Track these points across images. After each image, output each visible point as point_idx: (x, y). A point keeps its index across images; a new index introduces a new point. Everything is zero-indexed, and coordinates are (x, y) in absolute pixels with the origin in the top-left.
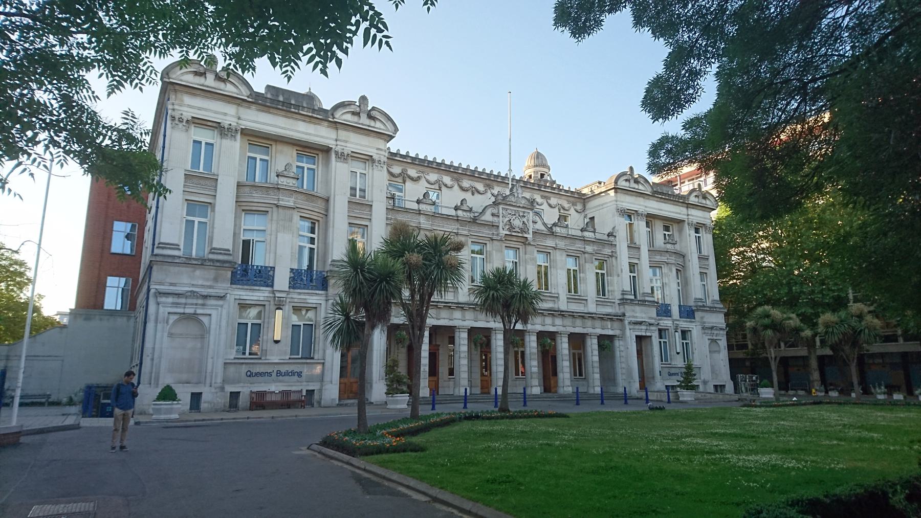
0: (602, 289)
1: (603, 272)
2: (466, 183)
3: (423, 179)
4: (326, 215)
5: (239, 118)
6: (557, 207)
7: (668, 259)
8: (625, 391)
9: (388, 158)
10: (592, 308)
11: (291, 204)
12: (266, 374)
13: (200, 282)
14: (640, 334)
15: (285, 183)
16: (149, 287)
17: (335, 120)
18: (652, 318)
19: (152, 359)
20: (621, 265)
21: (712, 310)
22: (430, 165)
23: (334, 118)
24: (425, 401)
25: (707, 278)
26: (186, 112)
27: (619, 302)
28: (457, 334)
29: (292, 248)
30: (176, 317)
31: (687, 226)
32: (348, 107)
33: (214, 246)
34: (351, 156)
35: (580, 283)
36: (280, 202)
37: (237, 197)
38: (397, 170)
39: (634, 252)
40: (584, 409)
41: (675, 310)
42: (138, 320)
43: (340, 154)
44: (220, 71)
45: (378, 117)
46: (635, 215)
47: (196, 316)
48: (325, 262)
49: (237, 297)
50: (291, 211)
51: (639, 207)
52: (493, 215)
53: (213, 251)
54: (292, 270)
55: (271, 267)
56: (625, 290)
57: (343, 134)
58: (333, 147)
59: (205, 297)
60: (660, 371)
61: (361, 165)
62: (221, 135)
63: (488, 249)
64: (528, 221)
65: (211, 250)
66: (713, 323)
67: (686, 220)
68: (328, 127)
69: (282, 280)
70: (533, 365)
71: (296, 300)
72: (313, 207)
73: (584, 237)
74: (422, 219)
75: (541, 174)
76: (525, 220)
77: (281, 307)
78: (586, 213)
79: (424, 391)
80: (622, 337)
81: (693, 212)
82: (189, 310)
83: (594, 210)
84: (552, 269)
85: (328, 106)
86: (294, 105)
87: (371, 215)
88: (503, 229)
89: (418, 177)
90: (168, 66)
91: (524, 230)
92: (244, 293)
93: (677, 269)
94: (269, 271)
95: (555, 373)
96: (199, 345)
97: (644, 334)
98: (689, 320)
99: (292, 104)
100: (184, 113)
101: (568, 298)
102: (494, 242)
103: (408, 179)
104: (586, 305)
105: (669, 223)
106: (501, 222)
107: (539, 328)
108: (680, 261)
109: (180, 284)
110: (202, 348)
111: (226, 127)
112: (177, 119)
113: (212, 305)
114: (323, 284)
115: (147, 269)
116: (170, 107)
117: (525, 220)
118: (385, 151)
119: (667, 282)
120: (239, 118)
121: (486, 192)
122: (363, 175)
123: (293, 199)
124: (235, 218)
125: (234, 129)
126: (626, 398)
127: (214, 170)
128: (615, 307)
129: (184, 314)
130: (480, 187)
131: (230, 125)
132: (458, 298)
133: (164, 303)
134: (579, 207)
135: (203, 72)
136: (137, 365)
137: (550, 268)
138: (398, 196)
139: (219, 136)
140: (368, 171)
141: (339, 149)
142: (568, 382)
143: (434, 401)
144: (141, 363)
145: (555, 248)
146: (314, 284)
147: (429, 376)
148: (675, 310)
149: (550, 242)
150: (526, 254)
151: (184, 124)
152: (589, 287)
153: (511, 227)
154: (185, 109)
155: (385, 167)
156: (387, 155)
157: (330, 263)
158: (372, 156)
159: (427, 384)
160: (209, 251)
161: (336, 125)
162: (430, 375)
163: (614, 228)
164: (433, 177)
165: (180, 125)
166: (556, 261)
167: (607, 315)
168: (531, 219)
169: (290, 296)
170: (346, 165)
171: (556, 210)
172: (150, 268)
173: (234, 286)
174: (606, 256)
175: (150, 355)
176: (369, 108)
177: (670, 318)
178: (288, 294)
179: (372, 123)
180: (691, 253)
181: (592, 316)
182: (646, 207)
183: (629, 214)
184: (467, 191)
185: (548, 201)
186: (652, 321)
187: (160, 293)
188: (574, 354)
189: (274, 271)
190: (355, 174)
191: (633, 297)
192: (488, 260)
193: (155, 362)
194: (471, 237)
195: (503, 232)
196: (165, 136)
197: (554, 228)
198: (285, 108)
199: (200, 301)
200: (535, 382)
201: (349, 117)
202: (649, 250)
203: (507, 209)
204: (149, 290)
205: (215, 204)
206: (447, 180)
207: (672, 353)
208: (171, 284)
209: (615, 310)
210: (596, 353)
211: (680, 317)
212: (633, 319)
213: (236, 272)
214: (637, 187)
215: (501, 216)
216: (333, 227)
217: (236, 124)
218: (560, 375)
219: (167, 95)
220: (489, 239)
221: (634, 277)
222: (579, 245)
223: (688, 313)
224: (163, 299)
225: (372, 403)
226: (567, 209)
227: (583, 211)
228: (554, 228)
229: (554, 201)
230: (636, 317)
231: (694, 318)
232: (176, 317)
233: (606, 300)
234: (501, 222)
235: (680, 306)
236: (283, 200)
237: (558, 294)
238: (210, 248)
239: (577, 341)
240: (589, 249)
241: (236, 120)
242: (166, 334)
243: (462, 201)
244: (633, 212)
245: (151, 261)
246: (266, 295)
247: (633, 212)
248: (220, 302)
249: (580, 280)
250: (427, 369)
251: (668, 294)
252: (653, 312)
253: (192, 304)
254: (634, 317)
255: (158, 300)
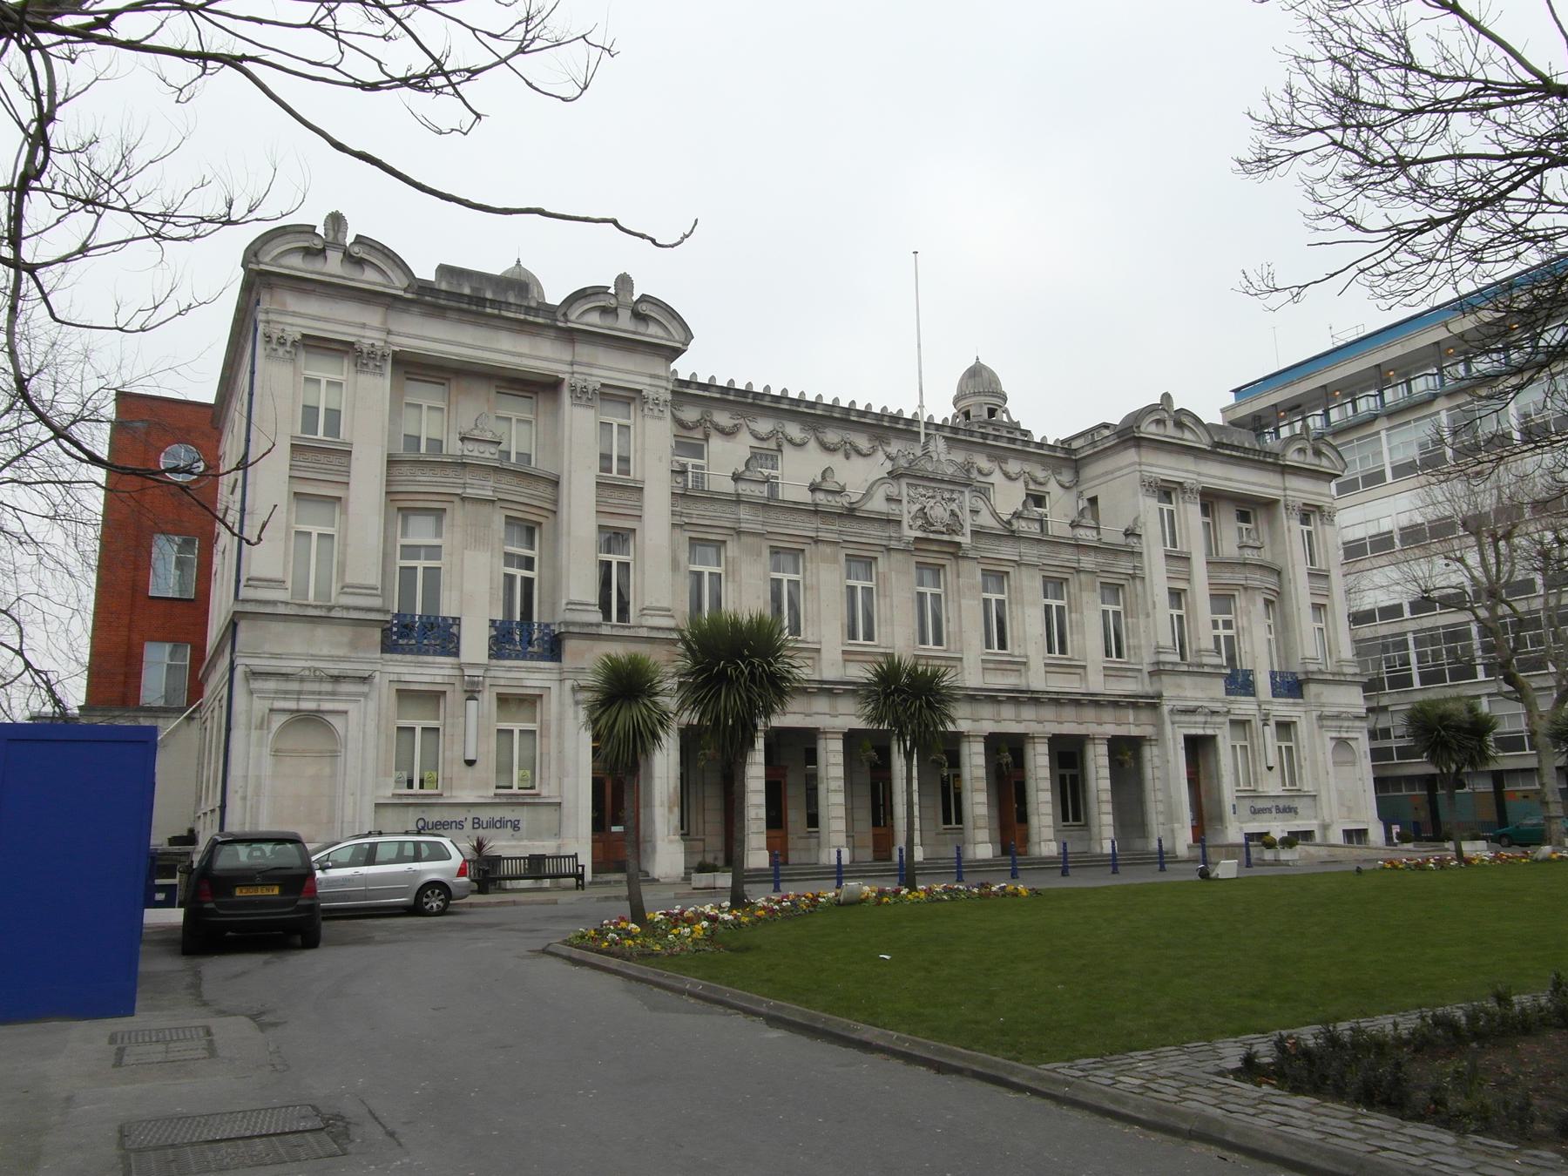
0: (1115, 644)
1: (1060, 603)
2: (832, 436)
3: (745, 428)
4: (555, 512)
5: (389, 332)
6: (1022, 479)
7: (1246, 579)
8: (1160, 846)
9: (673, 392)
10: (1096, 683)
11: (488, 493)
12: (454, 824)
13: (325, 651)
14: (1193, 731)
15: (476, 453)
16: (232, 662)
17: (570, 325)
18: (1217, 700)
19: (244, 798)
20: (1152, 595)
21: (1338, 681)
22: (758, 402)
23: (567, 321)
24: (758, 876)
25: (1326, 616)
26: (292, 325)
27: (1151, 669)
28: (821, 745)
29: (491, 579)
30: (284, 718)
31: (1284, 511)
32: (593, 298)
33: (349, 580)
34: (601, 393)
35: (1071, 634)
36: (468, 491)
37: (389, 483)
38: (691, 414)
39: (1179, 566)
40: (1077, 881)
41: (1263, 683)
42: (208, 724)
43: (578, 390)
44: (352, 244)
45: (653, 314)
46: (1179, 490)
47: (320, 715)
48: (554, 604)
49: (395, 678)
50: (487, 509)
51: (1185, 475)
52: (889, 499)
53: (345, 589)
54: (493, 622)
55: (454, 619)
56: (1161, 644)
57: (584, 352)
58: (566, 377)
59: (336, 679)
60: (1234, 806)
61: (620, 409)
62: (356, 365)
63: (880, 570)
64: (961, 508)
65: (342, 589)
66: (1339, 705)
67: (1282, 499)
68: (556, 338)
69: (475, 643)
70: (978, 801)
71: (502, 682)
72: (532, 496)
73: (1076, 540)
74: (744, 513)
75: (989, 409)
76: (954, 506)
77: (476, 695)
78: (1081, 489)
79: (757, 856)
80: (1158, 740)
81: (1295, 483)
82: (308, 705)
83: (1097, 482)
84: (1014, 606)
85: (554, 297)
86: (491, 300)
87: (641, 508)
88: (910, 526)
89: (736, 425)
90: (254, 241)
91: (954, 526)
92: (404, 670)
93: (1266, 600)
94: (451, 626)
95: (1023, 817)
96: (327, 771)
97: (1200, 732)
98: (1291, 700)
99: (487, 299)
100: (287, 328)
101: (1047, 665)
102: (892, 553)
103: (713, 432)
104: (1084, 678)
105: (1249, 508)
106: (905, 512)
107: (989, 727)
108: (1270, 581)
109: (288, 654)
110: (333, 775)
111: (365, 350)
112: (274, 341)
113: (348, 694)
114: (553, 648)
115: (227, 628)
116: (261, 317)
117: (954, 506)
118: (668, 380)
119: (1245, 625)
120: (389, 332)
121: (874, 450)
122: (625, 430)
123: (491, 483)
124: (385, 524)
125: (379, 353)
126: (1163, 858)
127: (344, 434)
128: (1142, 680)
129: (298, 711)
130: (863, 442)
131: (373, 345)
132: (821, 670)
133: (262, 691)
134: (1066, 477)
135: (320, 247)
136: (213, 811)
137: (1010, 603)
138: (694, 466)
139: (352, 368)
140: (634, 418)
141: (578, 381)
142: (1049, 833)
143: (776, 874)
144: (223, 807)
145: (1018, 564)
146: (536, 649)
147: (768, 827)
148: (1263, 683)
149: (1007, 551)
150: (958, 576)
151: (288, 349)
152: (1088, 640)
153: (927, 523)
154: (289, 320)
155: (668, 414)
156: (670, 387)
157: (564, 607)
158: (641, 391)
159: (763, 843)
160: (339, 590)
161: (571, 336)
162: (768, 827)
163: (1136, 519)
164: (764, 426)
165: (281, 351)
166: (1022, 591)
167: (1126, 696)
168: (967, 504)
169: (492, 673)
170: (591, 413)
171: (1020, 484)
172: (232, 626)
173: (387, 656)
174: (1123, 576)
175: (240, 791)
176: (635, 298)
177: (1252, 699)
178: (487, 670)
179: (642, 329)
180: (1293, 566)
181: (1095, 702)
182: (1199, 474)
183: (1165, 491)
184: (835, 450)
185: (1003, 466)
186: (1217, 706)
187: (254, 673)
188: (1062, 778)
189: (459, 625)
190: (609, 427)
191: (1177, 658)
192: (881, 592)
193: (248, 803)
194: (845, 545)
195: (911, 533)
196: (253, 373)
197: (1014, 522)
198: (474, 308)
199: (327, 687)
200: (983, 835)
201: (594, 318)
202: (1207, 563)
203: (916, 486)
204: (232, 669)
205: (347, 500)
206: (794, 430)
207: (1258, 768)
208: (274, 656)
209: (1143, 684)
210: (1106, 772)
211: (1274, 696)
212: (1180, 705)
213: (391, 629)
214: (1180, 435)
215: (905, 501)
216: (569, 534)
217: (382, 344)
218: (1034, 821)
219: (254, 295)
220: (882, 549)
221: (1180, 617)
222: (1066, 556)
223: (1291, 685)
224: (257, 685)
225: (658, 880)
226: (1042, 480)
227: (1075, 484)
228: (1014, 522)
229: (1013, 466)
230: (1185, 699)
231: (1302, 696)
232: (284, 718)
233: (1124, 666)
234: (905, 512)
235: (1273, 674)
236: (472, 486)
237: (1027, 657)
238: (340, 585)
239: (1068, 754)
240: (1088, 561)
241: (383, 336)
242: (267, 751)
243: (824, 472)
244: (1174, 486)
245: (235, 613)
246: (447, 672)
247: (1174, 486)
248: (365, 688)
249: (1071, 626)
250: (763, 813)
251: (1248, 649)
252: (1218, 688)
253: (313, 693)
254: (1179, 698)
255: (251, 686)
